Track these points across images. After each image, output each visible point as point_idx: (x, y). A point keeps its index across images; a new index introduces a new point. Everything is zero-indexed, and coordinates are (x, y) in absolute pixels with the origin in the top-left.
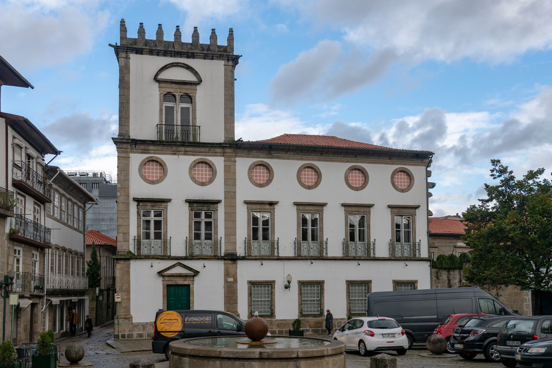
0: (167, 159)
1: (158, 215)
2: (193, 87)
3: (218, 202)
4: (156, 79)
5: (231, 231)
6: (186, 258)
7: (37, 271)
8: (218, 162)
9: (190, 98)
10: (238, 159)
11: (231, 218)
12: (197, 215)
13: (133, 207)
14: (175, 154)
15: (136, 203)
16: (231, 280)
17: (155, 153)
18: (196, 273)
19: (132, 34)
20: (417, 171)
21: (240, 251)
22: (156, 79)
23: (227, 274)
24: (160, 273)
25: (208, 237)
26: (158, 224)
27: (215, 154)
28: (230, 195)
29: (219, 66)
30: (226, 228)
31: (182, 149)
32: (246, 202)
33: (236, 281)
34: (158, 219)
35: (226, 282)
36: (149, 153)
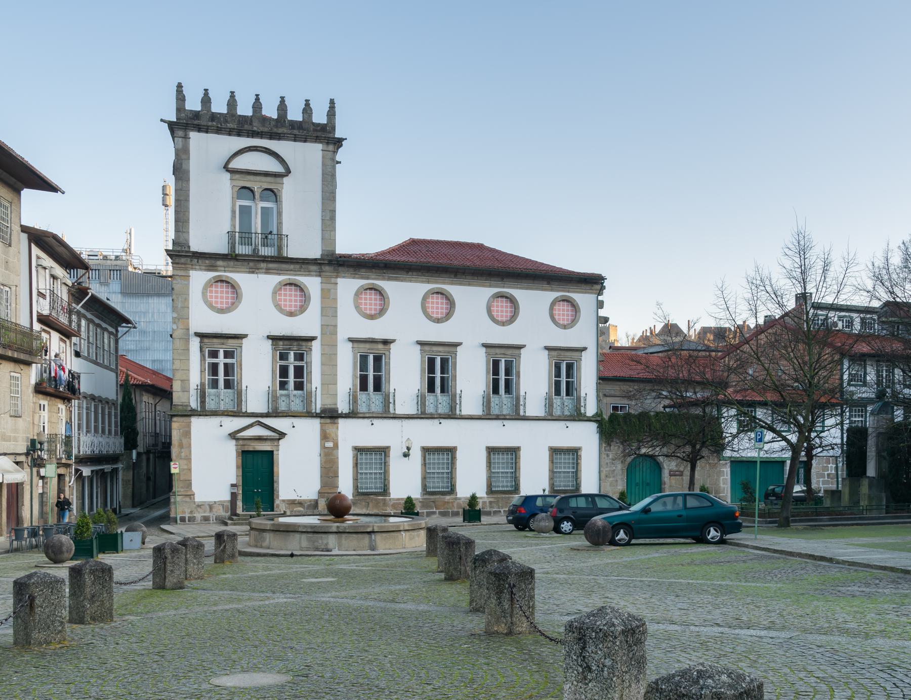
0: (241, 278)
1: (300, 357)
2: (278, 180)
3: (312, 339)
4: (226, 167)
5: (330, 380)
6: (267, 415)
7: (846, 366)
8: (313, 283)
9: (273, 194)
10: (340, 280)
11: (330, 360)
12: (283, 357)
13: (195, 343)
14: (253, 272)
15: (198, 340)
16: (329, 444)
17: (225, 271)
18: (282, 435)
19: (193, 104)
20: (584, 300)
21: (343, 406)
22: (226, 167)
23: (325, 437)
24: (233, 436)
25: (299, 386)
26: (228, 369)
27: (309, 273)
28: (329, 330)
29: (314, 151)
30: (323, 374)
31: (263, 265)
32: (352, 340)
33: (336, 446)
34: (228, 361)
35: (323, 447)
36: (216, 271)
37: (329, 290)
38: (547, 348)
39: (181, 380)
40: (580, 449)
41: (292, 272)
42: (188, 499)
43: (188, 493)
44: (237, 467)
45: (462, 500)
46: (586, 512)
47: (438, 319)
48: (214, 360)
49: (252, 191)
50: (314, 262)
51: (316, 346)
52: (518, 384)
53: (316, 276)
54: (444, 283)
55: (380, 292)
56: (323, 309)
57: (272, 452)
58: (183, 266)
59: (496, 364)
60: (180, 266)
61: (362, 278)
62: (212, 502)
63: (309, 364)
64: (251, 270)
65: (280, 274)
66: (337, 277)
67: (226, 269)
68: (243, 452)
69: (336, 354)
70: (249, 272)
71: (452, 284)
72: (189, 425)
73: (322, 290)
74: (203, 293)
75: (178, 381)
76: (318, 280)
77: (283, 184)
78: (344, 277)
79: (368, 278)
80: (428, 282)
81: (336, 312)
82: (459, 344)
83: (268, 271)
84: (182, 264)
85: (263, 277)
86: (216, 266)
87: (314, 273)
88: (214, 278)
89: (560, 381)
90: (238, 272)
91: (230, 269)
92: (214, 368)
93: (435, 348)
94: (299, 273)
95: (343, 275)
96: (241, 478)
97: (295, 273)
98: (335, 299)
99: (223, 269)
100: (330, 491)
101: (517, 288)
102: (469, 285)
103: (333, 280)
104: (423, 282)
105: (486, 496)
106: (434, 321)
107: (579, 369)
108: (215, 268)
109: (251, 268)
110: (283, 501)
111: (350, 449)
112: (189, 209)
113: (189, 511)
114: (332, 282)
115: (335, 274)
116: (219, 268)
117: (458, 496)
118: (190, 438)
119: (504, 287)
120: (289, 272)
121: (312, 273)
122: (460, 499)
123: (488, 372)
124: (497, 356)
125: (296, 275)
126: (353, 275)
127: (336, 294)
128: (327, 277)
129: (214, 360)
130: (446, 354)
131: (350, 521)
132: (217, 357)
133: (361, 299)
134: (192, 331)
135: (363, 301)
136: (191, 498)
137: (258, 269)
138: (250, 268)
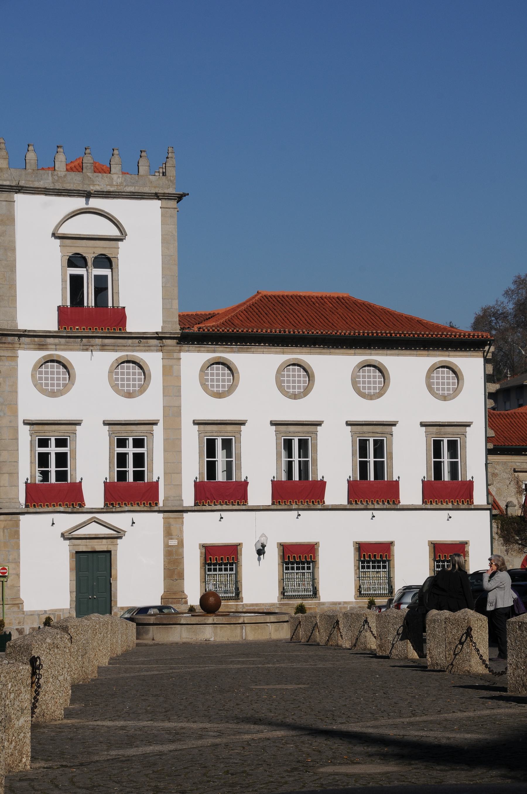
3: (155, 423)
4: (54, 235)
10: (183, 355)
14: (87, 350)
16: (173, 542)
22: (54, 235)
23: (168, 533)
26: (62, 459)
27: (148, 349)
32: (195, 423)
33: (181, 544)
35: (166, 546)
36: (47, 349)
37: (171, 367)
38: (273, 423)
39: (9, 473)
40: (467, 543)
41: (130, 348)
42: (15, 609)
43: (17, 602)
44: (71, 570)
45: (326, 605)
46: (251, 608)
47: (371, 396)
48: (122, 450)
49: (84, 259)
50: (159, 337)
51: (158, 431)
52: (391, 467)
53: (157, 351)
54: (301, 353)
55: (380, 369)
56: (165, 388)
57: (109, 552)
58: (10, 346)
59: (288, 444)
60: (6, 345)
61: (208, 351)
62: (41, 611)
63: (151, 451)
64: (85, 347)
65: (116, 351)
66: (180, 351)
67: (58, 347)
68: (77, 552)
69: (180, 439)
70: (83, 350)
71: (310, 353)
72: (17, 524)
73: (164, 366)
74: (32, 375)
75: (5, 475)
76: (159, 355)
77: (119, 248)
78: (188, 351)
79: (214, 351)
80: (283, 353)
81: (179, 391)
82: (242, 423)
83: (103, 348)
84: (9, 343)
85: (98, 354)
86: (46, 345)
87: (155, 348)
88: (44, 357)
89: (366, 462)
90: (71, 350)
91: (62, 347)
92: (122, 459)
93: (292, 428)
94: (138, 348)
95: (187, 348)
96: (75, 582)
97: (133, 348)
98: (179, 377)
99: (54, 347)
100: (174, 597)
101: (387, 355)
102: (330, 354)
103: (175, 355)
104: (276, 353)
105: (354, 600)
106: (290, 397)
107: (464, 447)
108: (45, 347)
109: (85, 345)
110: (122, 608)
111: (198, 547)
112: (16, 281)
113: (17, 622)
114: (175, 357)
115: (178, 348)
116: (50, 347)
117: (322, 600)
118: (18, 538)
119: (371, 354)
120: (126, 348)
121: (152, 348)
122: (323, 604)
123: (353, 455)
124: (364, 435)
125: (133, 351)
126: (198, 349)
127: (179, 371)
128: (169, 352)
129: (122, 450)
130: (304, 435)
131: (22, 621)
132: (125, 446)
133: (283, 376)
134: (21, 417)
135: (361, 380)
136: (19, 607)
137: (92, 346)
138: (83, 345)
